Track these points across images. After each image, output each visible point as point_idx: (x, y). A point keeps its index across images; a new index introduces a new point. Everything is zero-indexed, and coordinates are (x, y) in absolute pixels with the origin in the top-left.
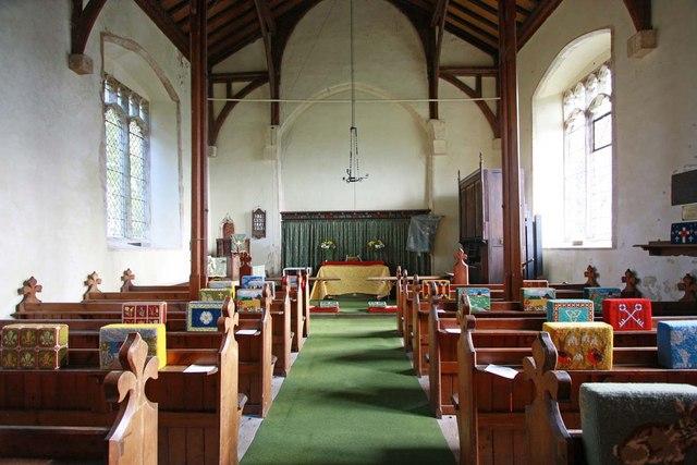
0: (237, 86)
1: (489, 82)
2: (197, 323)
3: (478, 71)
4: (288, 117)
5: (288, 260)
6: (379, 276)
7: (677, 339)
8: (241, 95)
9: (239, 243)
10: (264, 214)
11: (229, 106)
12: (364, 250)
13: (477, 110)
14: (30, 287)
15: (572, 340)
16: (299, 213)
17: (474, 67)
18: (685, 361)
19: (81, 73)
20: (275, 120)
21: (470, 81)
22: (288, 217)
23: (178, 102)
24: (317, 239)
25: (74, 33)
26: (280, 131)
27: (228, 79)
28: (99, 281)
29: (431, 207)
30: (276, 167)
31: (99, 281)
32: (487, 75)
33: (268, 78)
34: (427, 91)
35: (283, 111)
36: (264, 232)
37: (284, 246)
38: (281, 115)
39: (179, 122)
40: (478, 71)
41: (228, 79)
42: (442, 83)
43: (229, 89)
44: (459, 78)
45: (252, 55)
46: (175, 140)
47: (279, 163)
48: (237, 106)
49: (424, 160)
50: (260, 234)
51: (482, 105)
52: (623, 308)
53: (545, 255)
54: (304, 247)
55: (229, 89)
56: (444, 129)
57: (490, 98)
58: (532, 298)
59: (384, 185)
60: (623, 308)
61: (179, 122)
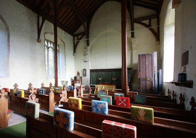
0: (80, 37)
1: (154, 21)
2: (40, 93)
3: (149, 18)
4: (91, 43)
5: (92, 82)
6: (113, 88)
7: (93, 105)
8: (80, 39)
9: (78, 78)
10: (86, 70)
11: (78, 42)
12: (111, 81)
13: (150, 32)
14: (30, 85)
15: (72, 101)
16: (94, 70)
17: (148, 17)
18: (95, 110)
19: (40, 43)
20: (88, 45)
21: (146, 22)
22: (92, 71)
23: (65, 44)
24: (101, 76)
25: (38, 34)
26: (89, 48)
27: (77, 35)
28: (44, 85)
29: (132, 67)
30: (89, 57)
31: (44, 85)
32: (153, 18)
33: (86, 34)
34: (130, 29)
35: (90, 41)
36: (86, 75)
37: (90, 78)
38: (89, 43)
39: (65, 49)
40: (149, 18)
41: (77, 35)
42: (136, 25)
43: (78, 37)
44: (143, 22)
45: (82, 29)
46: (64, 54)
47: (89, 56)
48: (80, 42)
49: (130, 52)
50: (85, 75)
51: (152, 30)
52: (125, 100)
53: (164, 84)
54: (95, 80)
55: (78, 37)
56: (136, 41)
57: (154, 27)
58: (116, 96)
59: (112, 61)
60: (120, 99)
61: (65, 49)
